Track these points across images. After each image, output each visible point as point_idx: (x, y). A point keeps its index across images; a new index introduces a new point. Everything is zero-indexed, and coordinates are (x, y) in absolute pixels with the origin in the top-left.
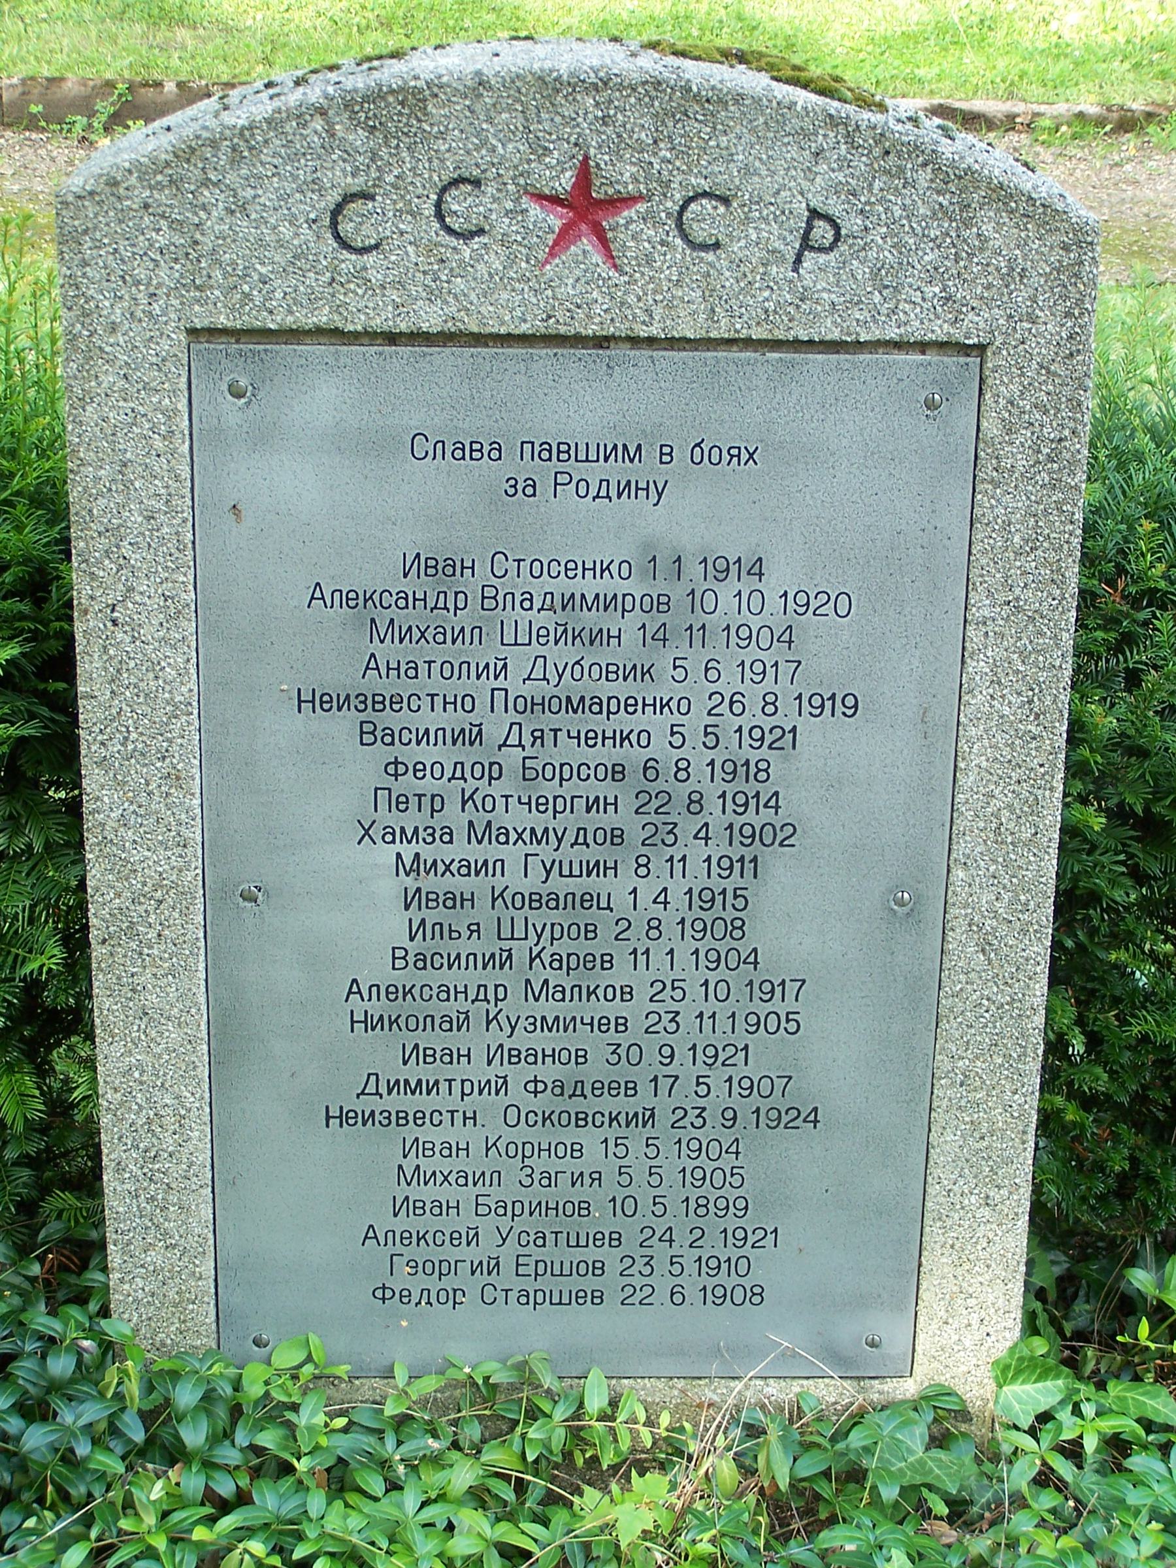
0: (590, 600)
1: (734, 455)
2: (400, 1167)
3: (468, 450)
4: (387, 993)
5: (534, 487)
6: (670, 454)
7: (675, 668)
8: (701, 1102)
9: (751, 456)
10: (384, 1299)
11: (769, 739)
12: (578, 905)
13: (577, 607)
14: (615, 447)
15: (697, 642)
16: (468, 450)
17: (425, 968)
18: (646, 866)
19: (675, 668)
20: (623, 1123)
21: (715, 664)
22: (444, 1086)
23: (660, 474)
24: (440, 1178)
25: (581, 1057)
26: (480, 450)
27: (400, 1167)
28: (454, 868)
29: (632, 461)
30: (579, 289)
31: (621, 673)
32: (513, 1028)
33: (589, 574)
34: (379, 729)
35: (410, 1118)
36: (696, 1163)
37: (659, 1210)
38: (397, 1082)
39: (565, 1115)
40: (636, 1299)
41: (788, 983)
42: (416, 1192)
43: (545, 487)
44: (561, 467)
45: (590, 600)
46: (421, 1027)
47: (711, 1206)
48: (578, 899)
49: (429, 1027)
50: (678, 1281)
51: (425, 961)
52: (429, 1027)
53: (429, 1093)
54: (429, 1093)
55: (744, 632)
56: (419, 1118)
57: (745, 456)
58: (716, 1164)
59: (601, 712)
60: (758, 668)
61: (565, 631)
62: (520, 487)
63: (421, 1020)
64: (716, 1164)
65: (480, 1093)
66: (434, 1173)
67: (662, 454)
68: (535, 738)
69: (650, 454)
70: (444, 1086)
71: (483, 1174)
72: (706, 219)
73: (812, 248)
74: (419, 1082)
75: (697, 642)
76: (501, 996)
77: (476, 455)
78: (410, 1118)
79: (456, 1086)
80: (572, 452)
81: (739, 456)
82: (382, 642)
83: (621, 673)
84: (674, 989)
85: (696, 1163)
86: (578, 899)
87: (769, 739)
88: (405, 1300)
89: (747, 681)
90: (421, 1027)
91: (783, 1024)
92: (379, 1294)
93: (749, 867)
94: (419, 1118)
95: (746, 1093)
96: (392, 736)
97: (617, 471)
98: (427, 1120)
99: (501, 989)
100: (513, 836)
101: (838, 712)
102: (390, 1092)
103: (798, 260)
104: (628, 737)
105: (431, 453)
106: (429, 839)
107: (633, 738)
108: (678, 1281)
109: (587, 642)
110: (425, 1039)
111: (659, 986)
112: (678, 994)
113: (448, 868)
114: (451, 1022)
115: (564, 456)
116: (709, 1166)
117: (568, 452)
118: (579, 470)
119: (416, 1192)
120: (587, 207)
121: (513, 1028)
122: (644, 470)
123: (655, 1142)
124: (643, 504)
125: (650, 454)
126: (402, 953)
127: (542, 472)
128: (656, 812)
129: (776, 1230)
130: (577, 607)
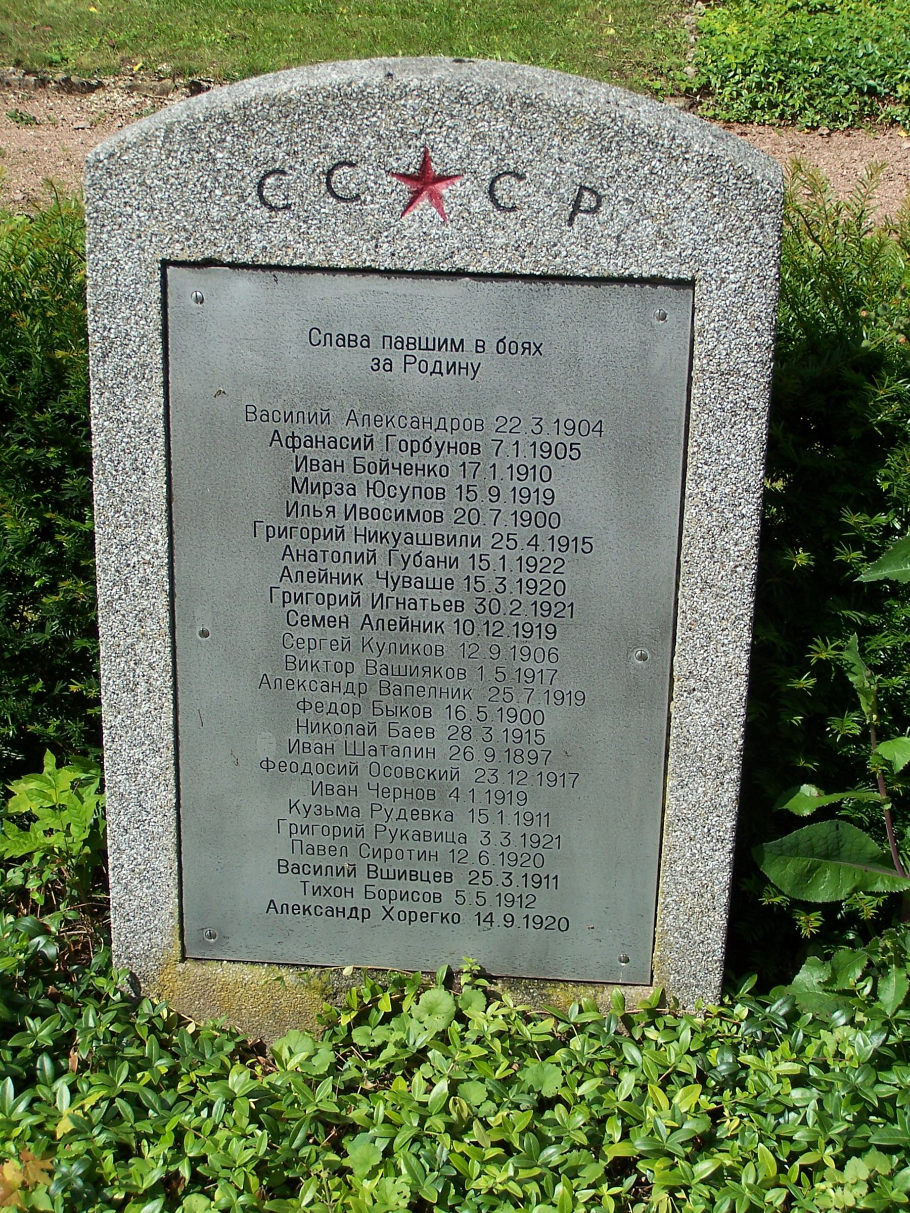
2: (294, 478)
4: (293, 909)
6: (483, 347)
8: (486, 868)
9: (538, 349)
13: (449, 348)
14: (446, 340)
17: (299, 873)
21: (511, 863)
23: (476, 359)
26: (355, 341)
27: (294, 478)
29: (457, 350)
30: (424, 232)
31: (445, 540)
34: (290, 864)
35: (327, 850)
42: (304, 499)
43: (398, 363)
44: (409, 352)
47: (525, 756)
50: (485, 848)
55: (525, 493)
57: (533, 349)
62: (381, 365)
63: (342, 556)
66: (319, 887)
67: (477, 346)
68: (525, 349)
69: (469, 345)
74: (323, 618)
77: (352, 344)
78: (327, 850)
80: (419, 875)
81: (529, 348)
83: (445, 540)
84: (484, 877)
86: (415, 690)
87: (540, 588)
89: (520, 636)
90: (342, 560)
93: (552, 882)
95: (490, 759)
96: (298, 868)
97: (446, 357)
99: (366, 912)
101: (573, 703)
103: (571, 221)
107: (449, 917)
108: (485, 848)
110: (312, 453)
111: (455, 750)
117: (414, 344)
119: (304, 499)
122: (467, 357)
123: (462, 893)
124: (465, 379)
125: (469, 345)
129: (572, 604)
130: (449, 348)
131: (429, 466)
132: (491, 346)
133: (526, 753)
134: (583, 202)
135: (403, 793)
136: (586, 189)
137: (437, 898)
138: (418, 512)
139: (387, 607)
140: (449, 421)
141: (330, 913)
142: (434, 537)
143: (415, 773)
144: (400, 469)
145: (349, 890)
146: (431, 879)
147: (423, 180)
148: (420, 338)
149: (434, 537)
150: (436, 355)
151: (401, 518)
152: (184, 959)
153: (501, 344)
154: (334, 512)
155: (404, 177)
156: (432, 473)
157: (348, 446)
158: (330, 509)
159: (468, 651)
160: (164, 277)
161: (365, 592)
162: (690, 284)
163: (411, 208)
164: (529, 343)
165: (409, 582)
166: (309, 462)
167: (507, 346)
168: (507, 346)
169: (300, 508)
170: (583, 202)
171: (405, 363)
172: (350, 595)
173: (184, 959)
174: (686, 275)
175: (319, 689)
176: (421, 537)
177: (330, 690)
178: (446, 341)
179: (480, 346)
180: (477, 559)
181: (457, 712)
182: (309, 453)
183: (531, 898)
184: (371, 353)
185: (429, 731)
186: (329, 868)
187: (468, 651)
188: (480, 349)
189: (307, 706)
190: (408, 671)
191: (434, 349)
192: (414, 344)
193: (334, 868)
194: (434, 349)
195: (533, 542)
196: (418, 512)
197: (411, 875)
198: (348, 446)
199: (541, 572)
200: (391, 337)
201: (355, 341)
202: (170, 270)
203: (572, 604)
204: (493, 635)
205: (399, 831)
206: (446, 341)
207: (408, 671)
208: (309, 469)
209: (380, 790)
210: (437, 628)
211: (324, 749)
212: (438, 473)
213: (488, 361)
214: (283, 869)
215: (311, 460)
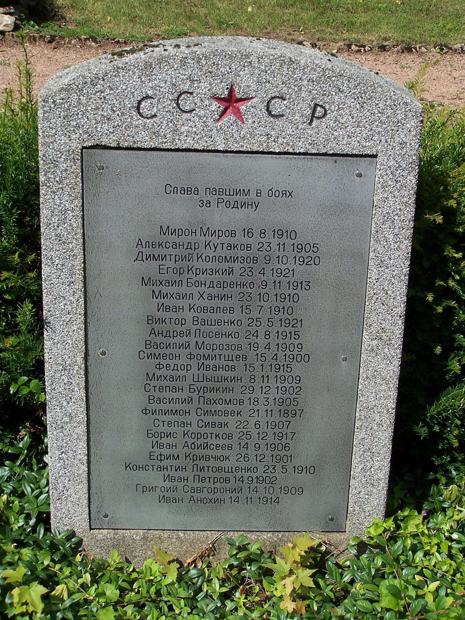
1: (284, 193)
5: (198, 191)
7: (283, 469)
9: (290, 194)
10: (146, 410)
11: (306, 261)
19: (283, 469)
20: (229, 380)
25: (231, 272)
28: (168, 378)
30: (226, 133)
32: (216, 248)
33: (224, 336)
36: (283, 385)
37: (270, 324)
39: (221, 400)
40: (241, 426)
41: (304, 282)
48: (222, 309)
51: (160, 400)
56: (165, 356)
57: (288, 194)
58: (290, 374)
59: (220, 287)
61: (207, 445)
64: (290, 374)
65: (203, 274)
66: (167, 294)
69: (253, 193)
71: (167, 491)
73: (318, 118)
80: (224, 192)
81: (286, 194)
85: (283, 385)
86: (222, 309)
87: (306, 261)
88: (168, 368)
89: (276, 439)
91: (292, 402)
92: (158, 367)
94: (165, 356)
95: (264, 287)
98: (168, 357)
100: (212, 402)
102: (147, 259)
103: (312, 121)
104: (233, 322)
105: (172, 192)
106: (227, 349)
107: (233, 335)
109: (221, 392)
112: (258, 324)
113: (161, 283)
116: (287, 375)
118: (226, 198)
121: (216, 248)
124: (250, 210)
125: (253, 193)
127: (213, 199)
128: (243, 428)
129: (258, 410)
133: (290, 412)
134: (316, 113)
135: (225, 490)
136: (318, 105)
138: (230, 400)
139: (234, 189)
140: (172, 333)
141: (174, 247)
143: (230, 347)
146: (234, 359)
150: (236, 198)
152: (91, 529)
153: (270, 191)
155: (219, 99)
156: (249, 471)
159: (261, 436)
161: (193, 341)
162: (375, 156)
163: (223, 118)
166: (165, 307)
167: (274, 192)
168: (274, 192)
169: (181, 378)
170: (316, 113)
173: (91, 529)
176: (228, 191)
180: (259, 356)
181: (248, 233)
183: (263, 456)
185: (230, 435)
186: (177, 400)
187: (261, 436)
188: (258, 195)
189: (161, 366)
190: (235, 193)
191: (233, 195)
194: (233, 195)
195: (255, 335)
196: (230, 400)
197: (212, 425)
199: (292, 327)
201: (191, 191)
202: (84, 150)
203: (258, 410)
204: (265, 394)
207: (235, 193)
208: (164, 311)
212: (252, 471)
214: (152, 401)
215: (166, 306)
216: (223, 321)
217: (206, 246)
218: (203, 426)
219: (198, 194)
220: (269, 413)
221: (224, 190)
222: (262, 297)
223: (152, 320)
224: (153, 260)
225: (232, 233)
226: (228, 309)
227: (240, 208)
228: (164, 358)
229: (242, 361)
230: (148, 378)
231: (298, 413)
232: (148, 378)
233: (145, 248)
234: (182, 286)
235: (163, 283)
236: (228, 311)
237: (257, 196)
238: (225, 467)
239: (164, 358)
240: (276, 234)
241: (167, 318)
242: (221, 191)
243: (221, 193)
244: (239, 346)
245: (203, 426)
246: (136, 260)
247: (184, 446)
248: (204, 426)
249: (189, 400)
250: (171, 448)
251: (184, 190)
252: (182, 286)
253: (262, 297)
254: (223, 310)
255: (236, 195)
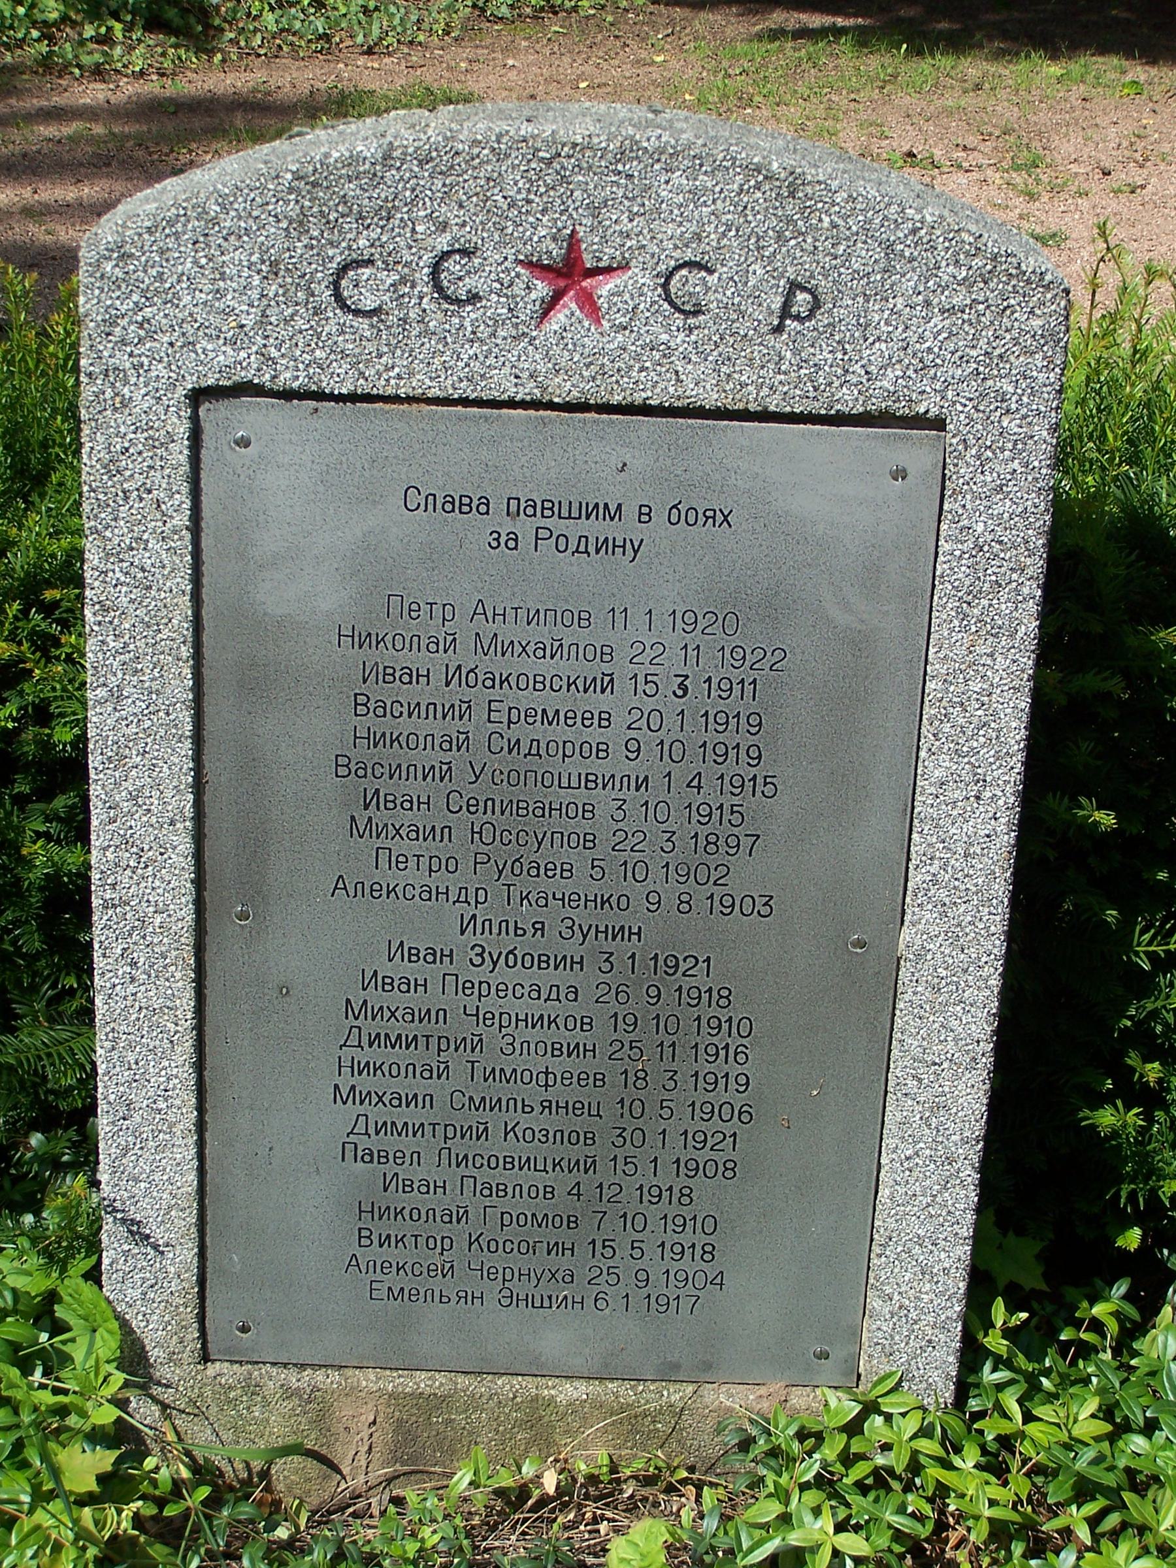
0: (551, 715)
3: (458, 504)
5: (487, 505)
9: (726, 517)
12: (439, 506)
15: (619, 624)
16: (458, 504)
18: (727, 997)
22: (422, 1041)
24: (387, 1014)
26: (469, 505)
29: (612, 519)
30: (568, 351)
37: (666, 1113)
38: (378, 1035)
44: (543, 523)
45: (551, 715)
46: (522, 783)
49: (430, 507)
52: (410, 1074)
53: (407, 1048)
54: (407, 1048)
57: (719, 518)
60: (721, 750)
62: (503, 540)
63: (407, 641)
65: (463, 1137)
66: (381, 1008)
67: (641, 514)
69: (630, 511)
70: (422, 1041)
72: (687, 283)
73: (797, 318)
75: (619, 624)
76: (481, 900)
79: (434, 1042)
80: (556, 509)
81: (714, 518)
82: (344, 1103)
83: (600, 781)
87: (683, 966)
95: (742, 1089)
97: (595, 528)
105: (422, 507)
109: (581, 689)
114: (431, 1071)
115: (547, 513)
117: (551, 509)
120: (568, 273)
124: (622, 560)
125: (630, 511)
126: (390, 981)
127: (525, 527)
128: (632, 850)
131: (602, 896)
132: (660, 516)
137: (588, 810)
140: (472, 891)
142: (583, 777)
144: (563, 900)
145: (424, 799)
147: (568, 273)
148: (560, 503)
149: (583, 777)
151: (592, 688)
153: (511, 956)
154: (542, 929)
157: (401, 713)
158: (537, 926)
160: (195, 420)
164: (715, 511)
165: (393, 675)
170: (798, 304)
171: (476, 863)
172: (437, 766)
174: (928, 406)
175: (417, 897)
177: (415, 807)
178: (597, 506)
179: (645, 514)
182: (400, 1236)
184: (475, 530)
190: (584, 512)
191: (580, 518)
192: (551, 509)
193: (439, 708)
194: (580, 518)
198: (401, 713)
199: (712, 1149)
200: (519, 499)
201: (469, 505)
205: (593, 930)
206: (597, 506)
207: (584, 512)
209: (481, 1017)
210: (375, 1070)
211: (432, 1186)
213: (658, 531)
216: (583, 898)
217: (506, 1134)
218: (461, 807)
219: (487, 513)
220: (620, 618)
221: (557, 505)
222: (666, 747)
223: (365, 705)
224: (543, 723)
225: (583, 619)
226: (596, 717)
227: (366, 1047)
228: (398, 1161)
229: (600, 726)
230: (355, 831)
231: (746, 842)
232: (355, 831)
233: (427, 718)
234: (445, 1023)
235: (386, 1099)
236: (558, 871)
237: (640, 521)
238: (560, 503)
239: (398, 1161)
240: (697, 1111)
241: (409, 1235)
242: (549, 507)
243: (547, 513)
244: (590, 777)
245: (461, 807)
246: (344, 1045)
247: (336, 888)
248: (506, 749)
249: (463, 710)
250: (412, 990)
251: (453, 503)
252: (445, 1023)
253: (666, 747)
254: (397, 862)
255: (588, 518)
